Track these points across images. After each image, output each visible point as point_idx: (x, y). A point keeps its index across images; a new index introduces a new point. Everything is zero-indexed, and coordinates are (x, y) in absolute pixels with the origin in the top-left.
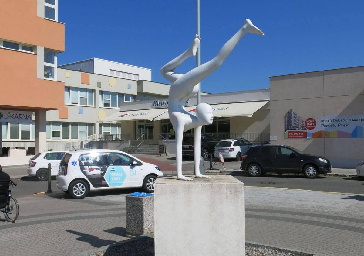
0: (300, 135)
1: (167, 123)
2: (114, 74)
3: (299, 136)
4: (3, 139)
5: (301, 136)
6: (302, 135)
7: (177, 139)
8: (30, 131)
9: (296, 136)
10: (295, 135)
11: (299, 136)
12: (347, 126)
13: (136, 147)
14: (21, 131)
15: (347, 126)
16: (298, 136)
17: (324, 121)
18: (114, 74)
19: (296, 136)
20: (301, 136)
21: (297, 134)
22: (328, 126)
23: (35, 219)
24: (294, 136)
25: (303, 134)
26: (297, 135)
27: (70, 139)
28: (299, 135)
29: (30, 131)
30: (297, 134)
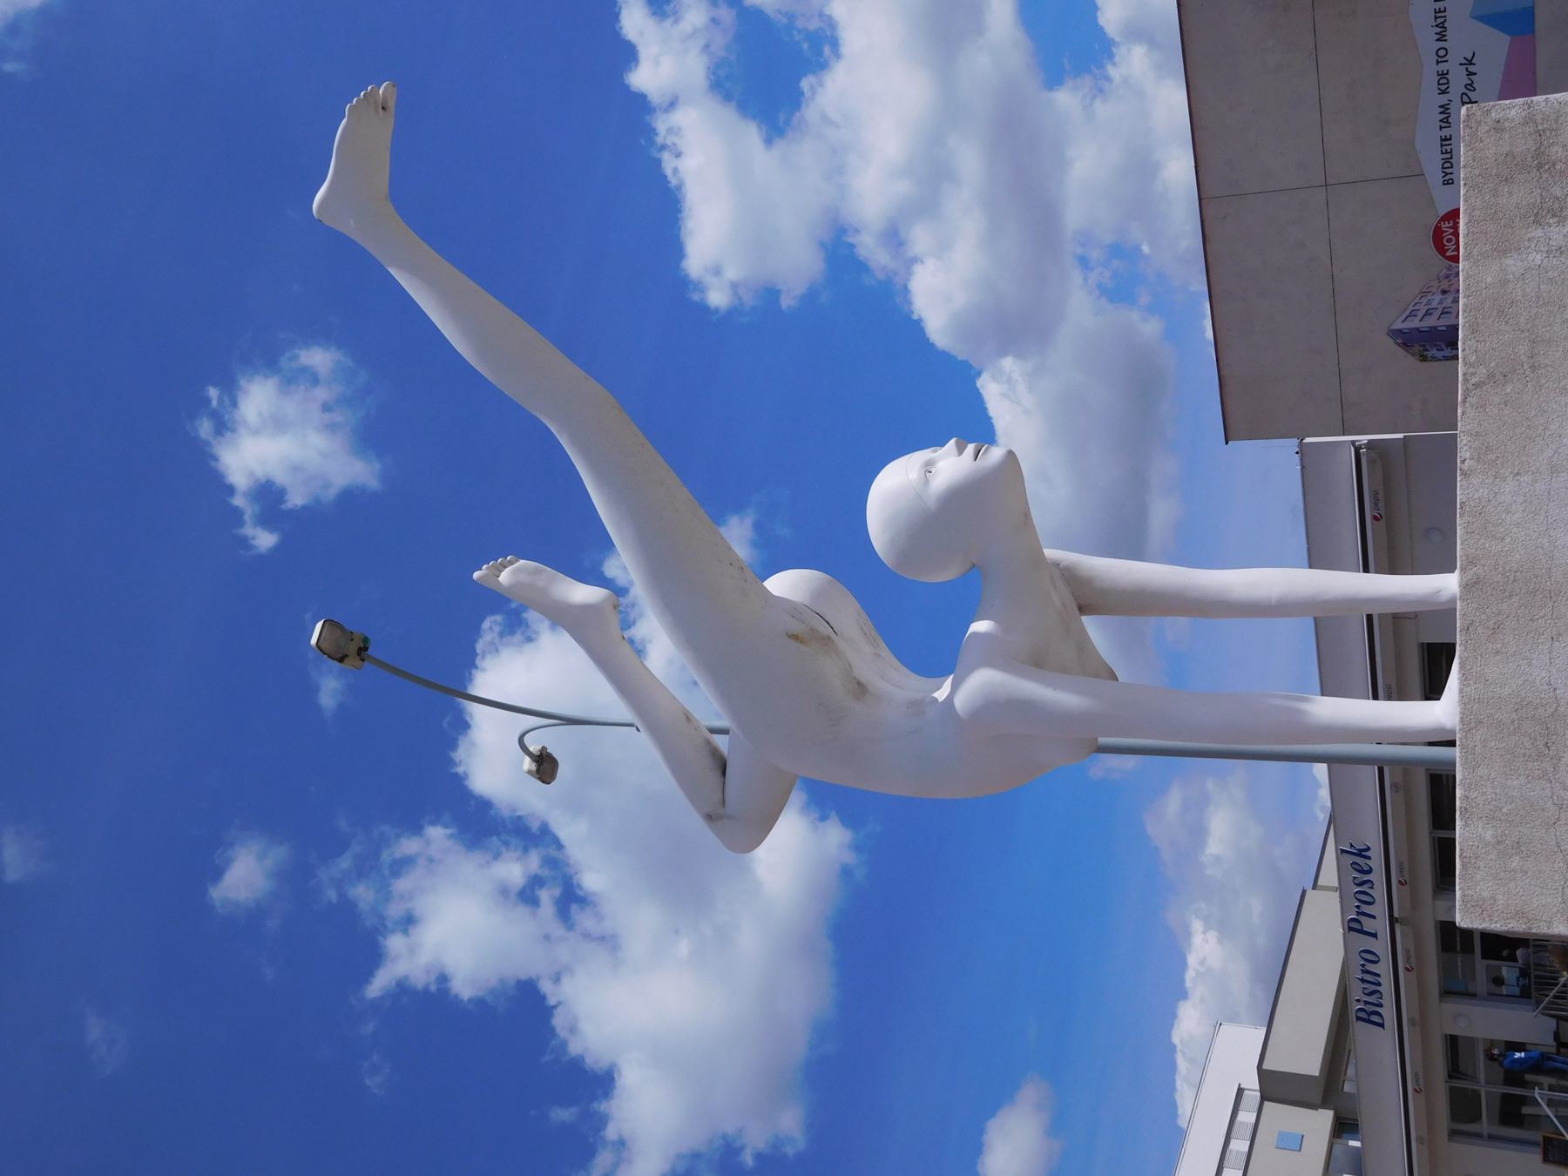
17: (1447, 174)
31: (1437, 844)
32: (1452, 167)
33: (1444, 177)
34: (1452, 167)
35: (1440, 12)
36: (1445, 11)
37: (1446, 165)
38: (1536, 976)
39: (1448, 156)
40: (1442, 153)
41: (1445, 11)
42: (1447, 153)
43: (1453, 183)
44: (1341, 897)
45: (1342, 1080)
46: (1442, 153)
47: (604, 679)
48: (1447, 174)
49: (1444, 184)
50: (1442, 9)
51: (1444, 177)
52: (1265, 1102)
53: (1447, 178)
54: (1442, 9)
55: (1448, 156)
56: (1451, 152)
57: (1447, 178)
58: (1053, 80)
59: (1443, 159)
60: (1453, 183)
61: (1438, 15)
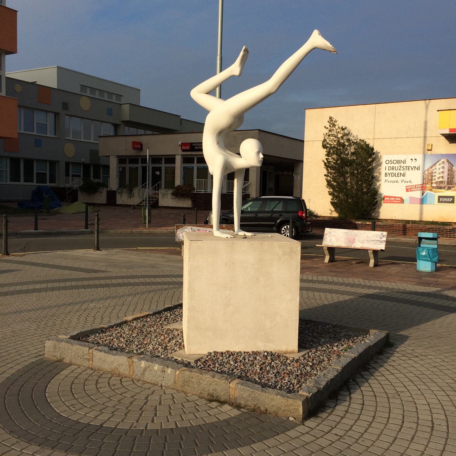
0: (397, 200)
1: (173, 168)
2: (86, 93)
3: (395, 201)
4: (421, 236)
5: (397, 202)
6: (398, 200)
7: (219, 196)
8: (46, 173)
9: (392, 201)
10: (391, 200)
11: (395, 201)
12: (410, 182)
13: (67, 193)
14: (36, 172)
15: (410, 182)
16: (394, 201)
17: (389, 174)
18: (86, 93)
19: (392, 201)
20: (397, 202)
21: (393, 199)
22: (392, 182)
23: (38, 286)
24: (389, 201)
25: (399, 199)
26: (393, 200)
27: (22, 182)
28: (395, 200)
29: (46, 173)
30: (393, 199)
31: (262, 172)
32: (392, 176)
33: (388, 173)
34: (392, 176)
35: (408, 168)
36: (408, 170)
37: (393, 174)
38: (203, 180)
39: (396, 175)
40: (398, 173)
41: (408, 170)
42: (398, 175)
43: (385, 176)
44: (56, 89)
45: (264, 239)
46: (398, 173)
47: (264, 234)
48: (389, 174)
49: (385, 173)
50: (409, 169)
51: (388, 173)
52: (54, 114)
53: (388, 174)
54: (409, 169)
55: (396, 175)
56: (398, 176)
57: (388, 174)
58: (115, 192)
59: (395, 173)
60: (385, 176)
61: (407, 168)
